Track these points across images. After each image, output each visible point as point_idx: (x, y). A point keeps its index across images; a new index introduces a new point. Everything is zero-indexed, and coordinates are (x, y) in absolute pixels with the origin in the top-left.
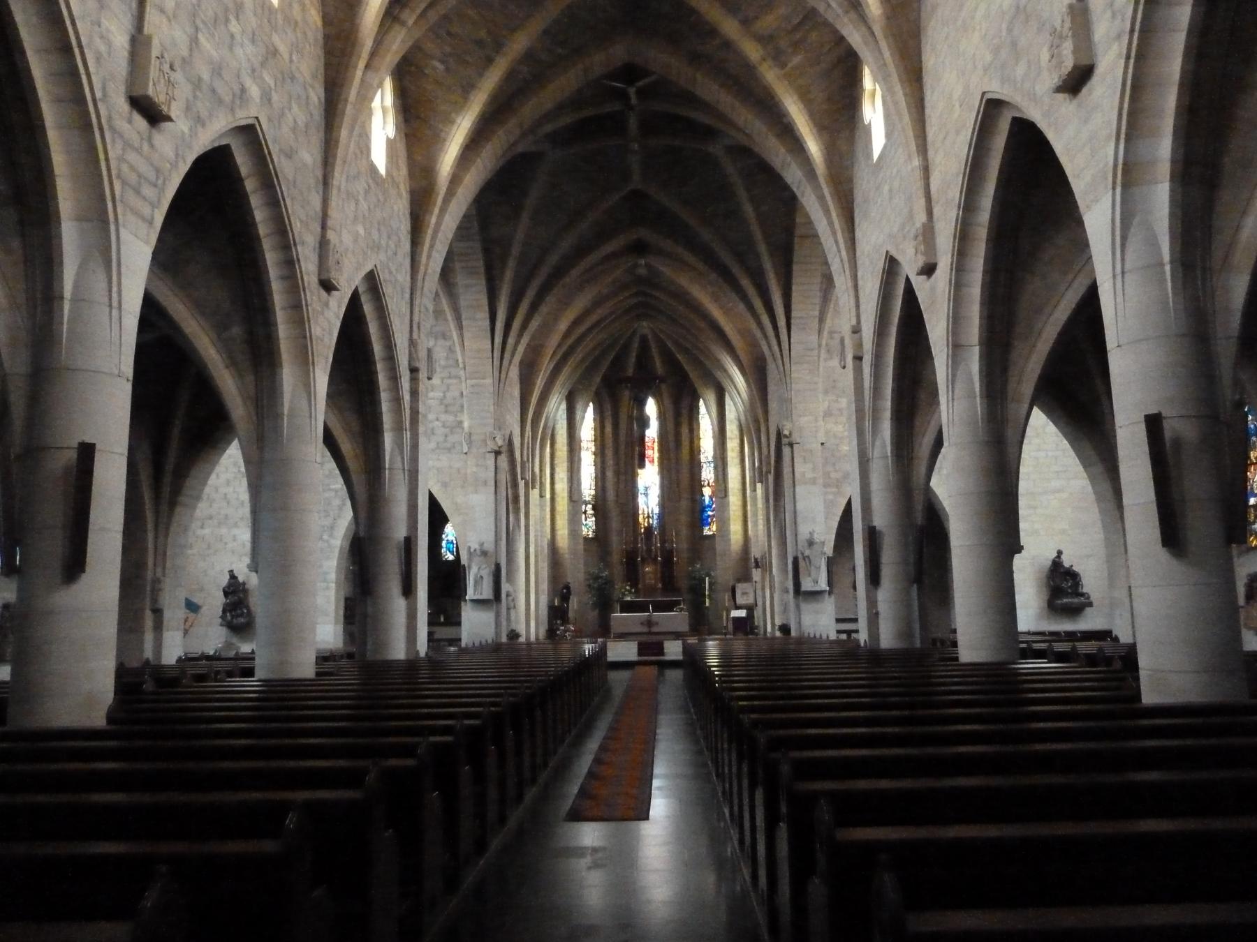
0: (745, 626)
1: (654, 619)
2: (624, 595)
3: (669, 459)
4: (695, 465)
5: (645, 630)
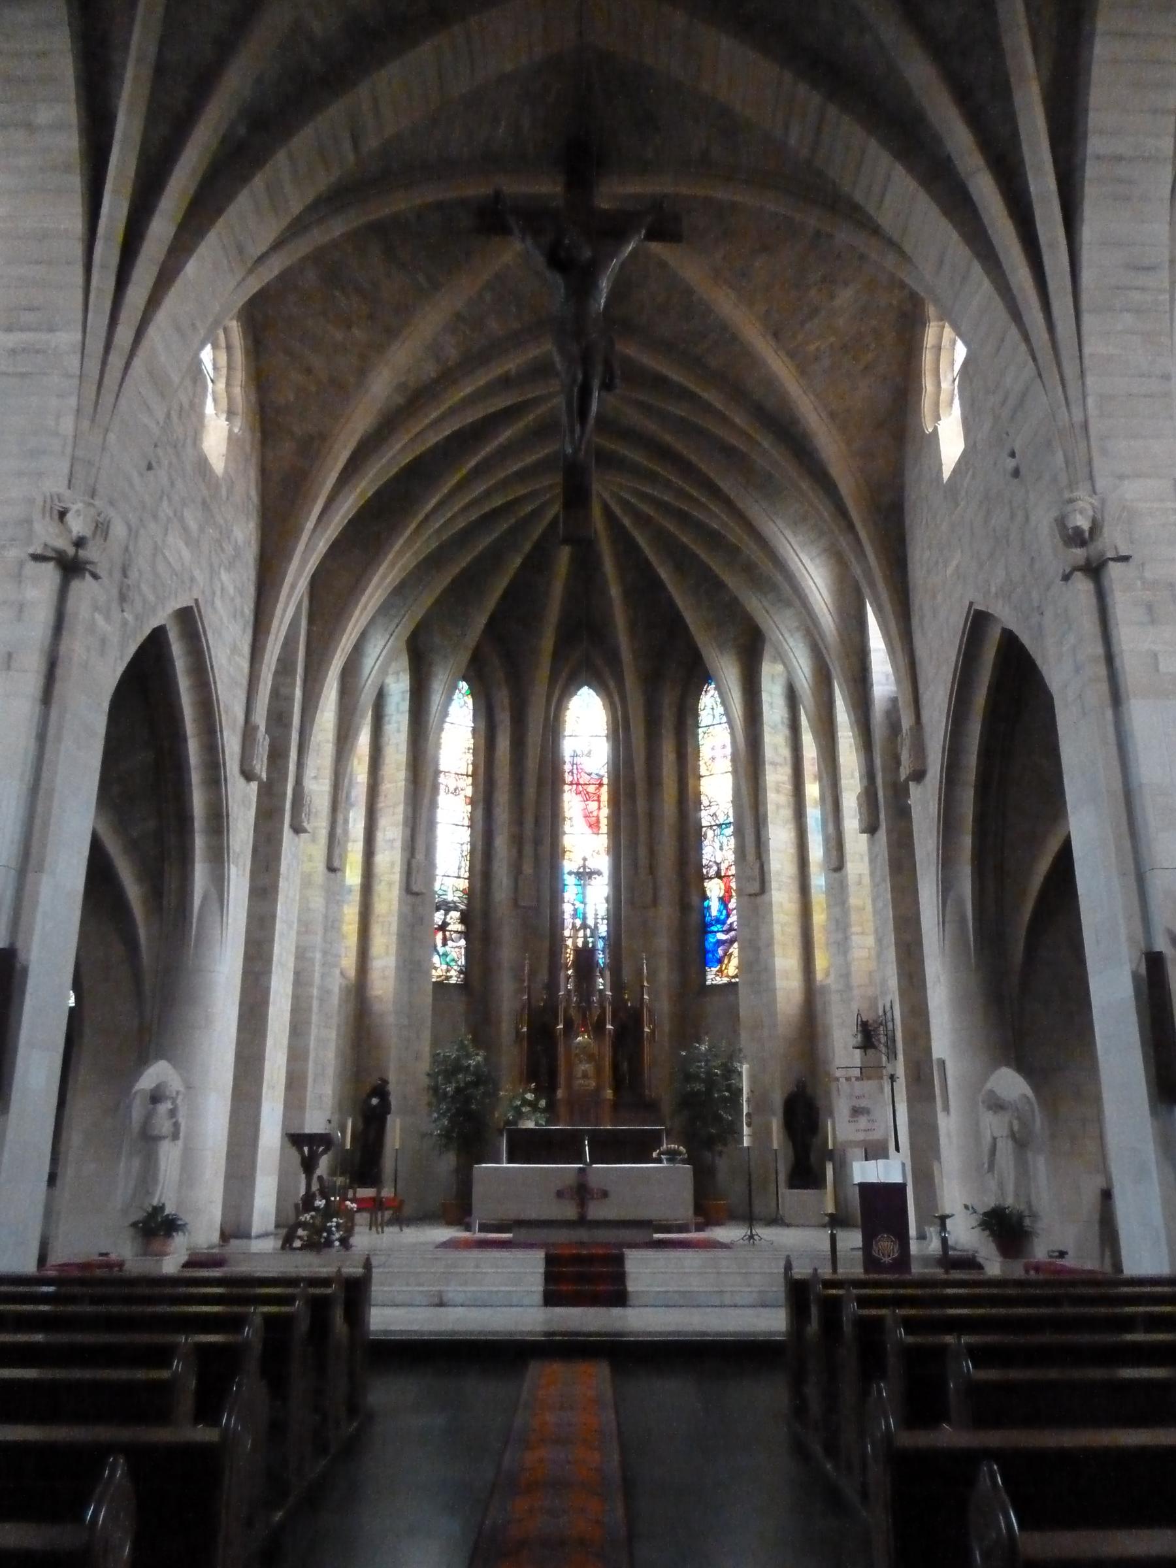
0: (882, 1208)
1: (594, 1182)
2: (519, 1115)
3: (633, 815)
4: (689, 836)
5: (569, 1211)
